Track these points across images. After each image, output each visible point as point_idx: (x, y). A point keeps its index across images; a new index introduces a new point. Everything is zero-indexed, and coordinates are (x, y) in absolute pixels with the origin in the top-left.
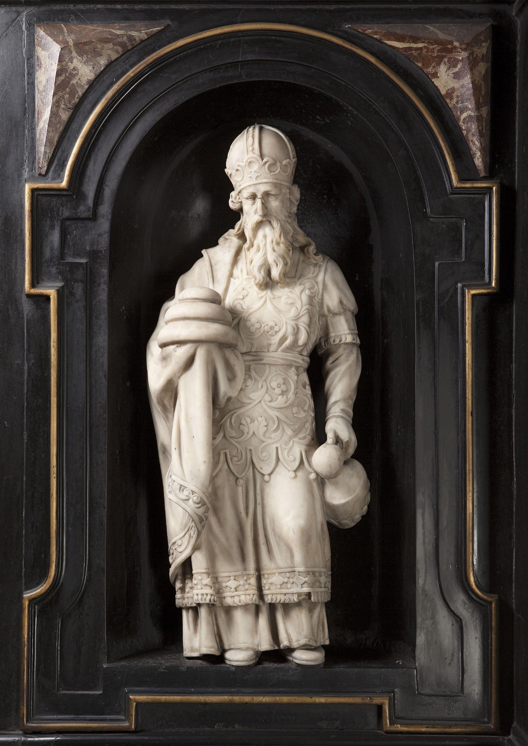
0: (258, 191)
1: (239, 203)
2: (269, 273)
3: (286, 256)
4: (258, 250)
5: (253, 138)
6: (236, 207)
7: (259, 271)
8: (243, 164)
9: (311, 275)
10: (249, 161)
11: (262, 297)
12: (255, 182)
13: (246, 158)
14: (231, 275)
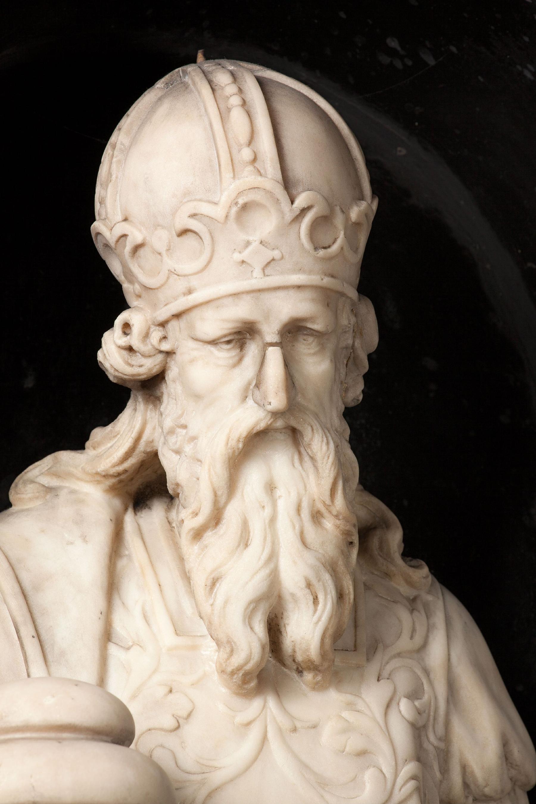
0: (267, 316)
1: (160, 358)
2: (274, 629)
3: (341, 567)
4: (244, 540)
5: (249, 114)
6: (142, 370)
7: (248, 618)
8: (218, 212)
9: (404, 643)
10: (241, 201)
11: (248, 724)
12: (257, 281)
13: (229, 189)
14: (107, 636)
